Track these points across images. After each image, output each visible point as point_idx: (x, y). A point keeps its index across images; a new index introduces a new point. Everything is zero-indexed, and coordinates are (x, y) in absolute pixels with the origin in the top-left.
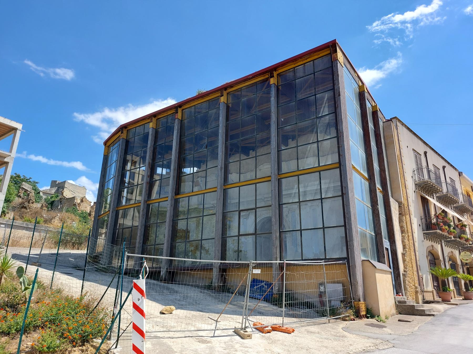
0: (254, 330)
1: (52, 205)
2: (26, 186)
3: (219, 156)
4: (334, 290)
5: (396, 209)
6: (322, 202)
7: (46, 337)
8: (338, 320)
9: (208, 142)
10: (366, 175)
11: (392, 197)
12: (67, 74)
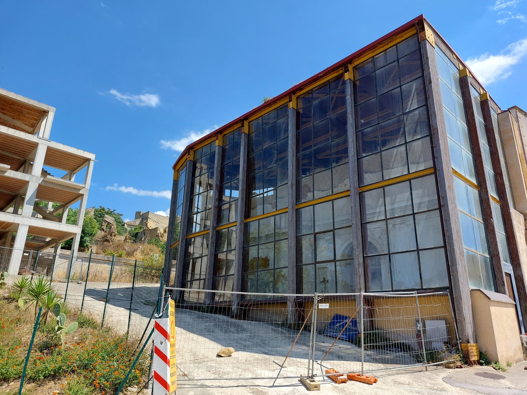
0: (326, 378)
1: (136, 237)
2: (109, 218)
3: (289, 170)
4: (437, 328)
5: (520, 223)
6: (414, 218)
7: (72, 383)
8: (439, 367)
10: (474, 181)
11: (515, 208)
12: (152, 100)
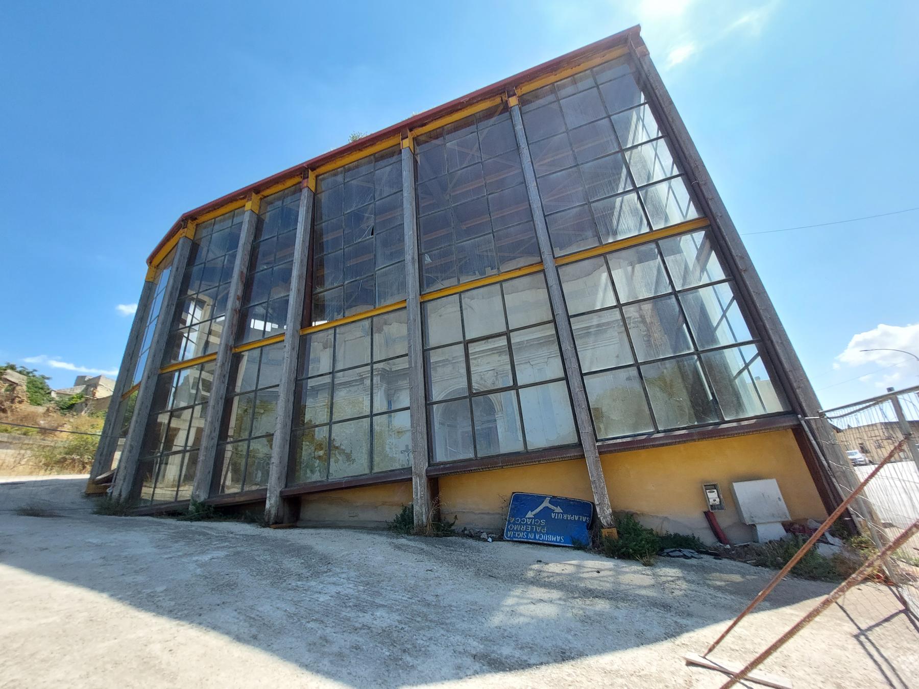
3: (406, 238)
9: (375, 223)
